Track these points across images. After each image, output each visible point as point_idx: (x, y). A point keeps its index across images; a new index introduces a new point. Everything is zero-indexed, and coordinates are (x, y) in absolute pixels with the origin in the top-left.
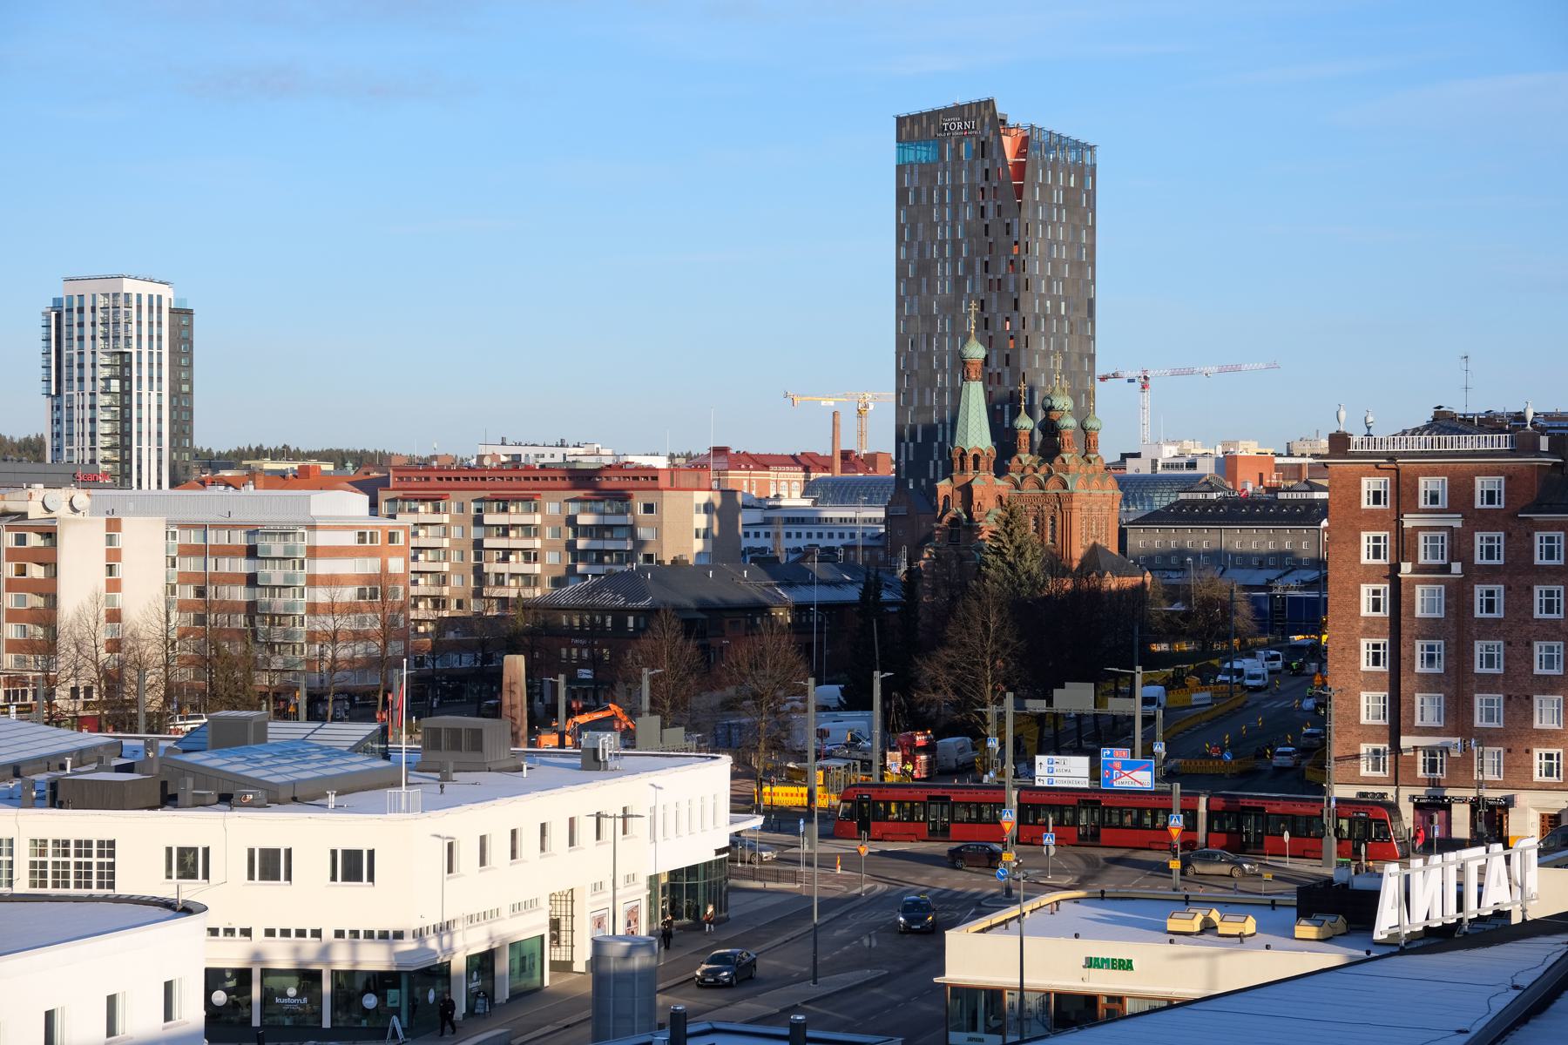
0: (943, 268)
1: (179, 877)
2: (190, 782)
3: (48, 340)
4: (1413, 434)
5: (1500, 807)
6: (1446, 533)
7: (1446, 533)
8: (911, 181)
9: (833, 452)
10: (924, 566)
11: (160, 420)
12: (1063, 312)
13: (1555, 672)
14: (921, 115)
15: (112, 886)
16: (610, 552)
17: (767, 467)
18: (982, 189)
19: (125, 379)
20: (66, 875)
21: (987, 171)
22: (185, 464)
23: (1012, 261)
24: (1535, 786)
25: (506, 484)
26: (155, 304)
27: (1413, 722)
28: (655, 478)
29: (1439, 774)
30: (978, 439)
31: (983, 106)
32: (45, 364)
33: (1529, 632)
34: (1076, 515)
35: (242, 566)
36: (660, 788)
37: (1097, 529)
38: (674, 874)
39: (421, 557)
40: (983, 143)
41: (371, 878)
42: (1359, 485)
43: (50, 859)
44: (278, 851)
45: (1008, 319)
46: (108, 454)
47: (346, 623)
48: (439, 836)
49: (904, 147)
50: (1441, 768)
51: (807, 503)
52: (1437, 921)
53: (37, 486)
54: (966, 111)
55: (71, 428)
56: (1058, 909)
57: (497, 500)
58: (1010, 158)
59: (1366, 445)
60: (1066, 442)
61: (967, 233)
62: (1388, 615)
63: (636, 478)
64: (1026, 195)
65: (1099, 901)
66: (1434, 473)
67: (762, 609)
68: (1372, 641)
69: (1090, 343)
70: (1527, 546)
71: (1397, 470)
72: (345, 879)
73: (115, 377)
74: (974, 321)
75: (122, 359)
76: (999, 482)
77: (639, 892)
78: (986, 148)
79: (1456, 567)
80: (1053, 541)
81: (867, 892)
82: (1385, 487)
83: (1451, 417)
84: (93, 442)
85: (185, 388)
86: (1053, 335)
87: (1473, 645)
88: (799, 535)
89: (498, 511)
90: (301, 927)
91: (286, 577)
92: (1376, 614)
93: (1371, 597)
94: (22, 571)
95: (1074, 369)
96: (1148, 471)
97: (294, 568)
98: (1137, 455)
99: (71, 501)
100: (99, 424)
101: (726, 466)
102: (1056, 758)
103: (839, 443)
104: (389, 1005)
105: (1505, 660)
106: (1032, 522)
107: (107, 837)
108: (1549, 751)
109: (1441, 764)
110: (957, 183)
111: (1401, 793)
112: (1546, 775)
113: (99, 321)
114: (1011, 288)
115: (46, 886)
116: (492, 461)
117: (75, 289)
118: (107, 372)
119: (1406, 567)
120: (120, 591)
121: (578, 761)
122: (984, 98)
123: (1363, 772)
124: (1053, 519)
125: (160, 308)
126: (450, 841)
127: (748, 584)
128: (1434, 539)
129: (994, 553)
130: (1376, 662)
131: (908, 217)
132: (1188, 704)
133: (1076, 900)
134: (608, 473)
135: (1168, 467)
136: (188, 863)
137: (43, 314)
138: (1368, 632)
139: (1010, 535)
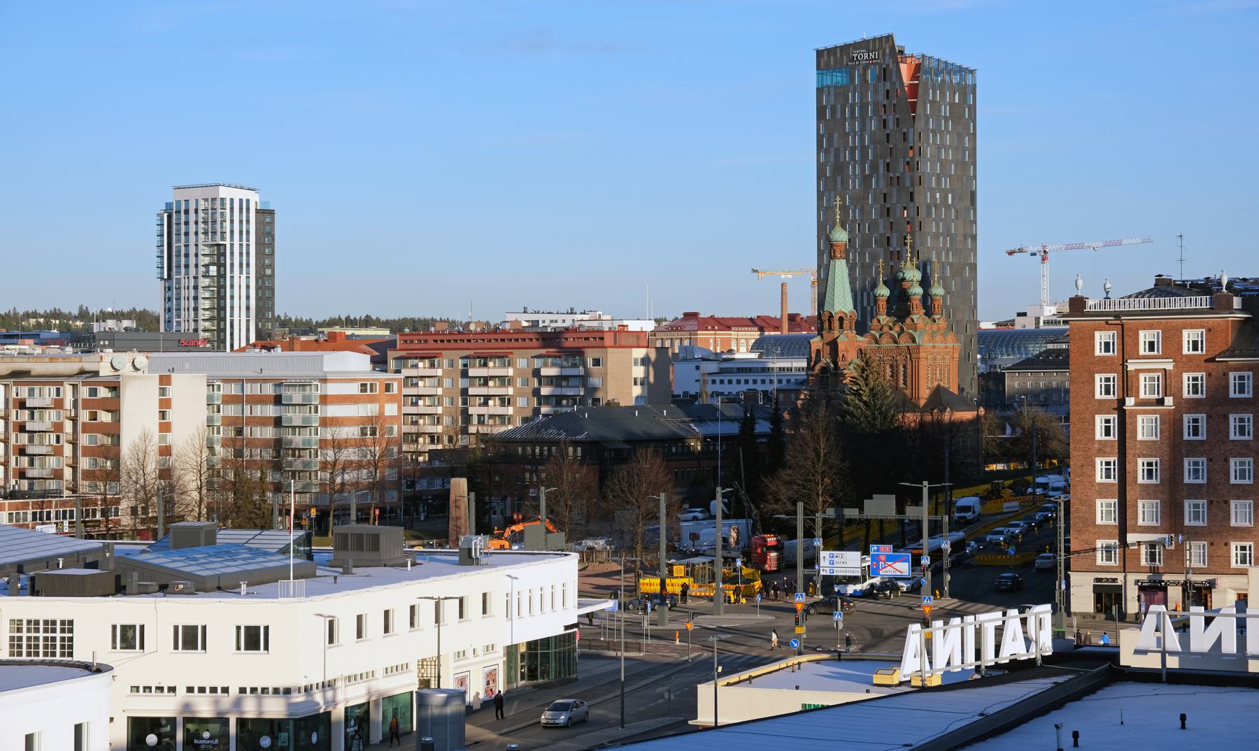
0: (854, 168)
1: (121, 648)
2: (135, 575)
3: (162, 235)
4: (1137, 297)
5: (1206, 588)
6: (1160, 374)
7: (1160, 374)
8: (828, 101)
9: (782, 315)
10: (802, 405)
11: (248, 297)
12: (950, 202)
13: (1246, 481)
14: (836, 48)
15: (71, 654)
16: (567, 397)
17: (729, 328)
18: (884, 106)
19: (221, 265)
20: (37, 646)
21: (888, 91)
22: (268, 332)
23: (908, 163)
24: (1232, 572)
25: (487, 344)
26: (244, 206)
27: (1137, 522)
28: (602, 339)
29: (1157, 563)
30: (843, 304)
31: (884, 40)
32: (159, 254)
33: (1227, 451)
34: (923, 363)
35: (271, 411)
36: (516, 578)
37: (941, 374)
38: (532, 645)
39: (421, 402)
40: (884, 69)
41: (204, 648)
42: (1093, 338)
43: (25, 635)
44: (258, 628)
45: (905, 208)
46: (207, 324)
47: (350, 454)
48: (321, 615)
49: (822, 74)
50: (1160, 559)
51: (754, 356)
52: (958, 667)
53: (108, 350)
54: (871, 44)
55: (179, 305)
56: (799, 668)
57: (478, 357)
58: (906, 80)
59: (1103, 307)
60: (915, 306)
61: (872, 141)
62: (1116, 439)
63: (587, 339)
64: (919, 109)
65: (837, 662)
66: (1151, 327)
67: (679, 440)
68: (1146, 460)
69: (972, 226)
70: (1223, 383)
71: (1122, 325)
72: (247, 648)
73: (213, 264)
74: (838, 212)
75: (219, 250)
76: (859, 338)
77: (499, 658)
78: (887, 74)
79: (1169, 401)
80: (905, 384)
81: (693, 659)
82: (1113, 339)
83: (1169, 282)
84: (196, 315)
85: (268, 272)
86: (942, 220)
87: (1183, 461)
88: (730, 382)
89: (480, 366)
90: (202, 685)
91: (304, 419)
92: (1108, 438)
93: (1104, 424)
94: (94, 417)
95: (960, 247)
96: (1033, 327)
97: (310, 412)
98: (1024, 314)
99: (133, 362)
100: (201, 301)
101: (696, 328)
102: (836, 553)
103: (786, 308)
104: (280, 744)
105: (1208, 473)
106: (888, 370)
107: (67, 618)
108: (1243, 544)
109: (1160, 555)
110: (864, 101)
111: (1128, 579)
112: (1241, 563)
113: (201, 220)
114: (908, 183)
115: (55, 656)
116: (476, 327)
117: (182, 194)
118: (207, 260)
119: (1130, 402)
120: (170, 432)
121: (457, 558)
122: (885, 33)
123: (1099, 562)
124: (905, 367)
125: (248, 209)
126: (331, 619)
127: (668, 421)
128: (1152, 379)
129: (853, 394)
130: (1108, 476)
131: (826, 129)
132: (1001, 511)
133: (818, 662)
134: (567, 335)
135: (1048, 323)
136: (128, 637)
137: (158, 215)
138: (1101, 453)
139: (866, 380)
